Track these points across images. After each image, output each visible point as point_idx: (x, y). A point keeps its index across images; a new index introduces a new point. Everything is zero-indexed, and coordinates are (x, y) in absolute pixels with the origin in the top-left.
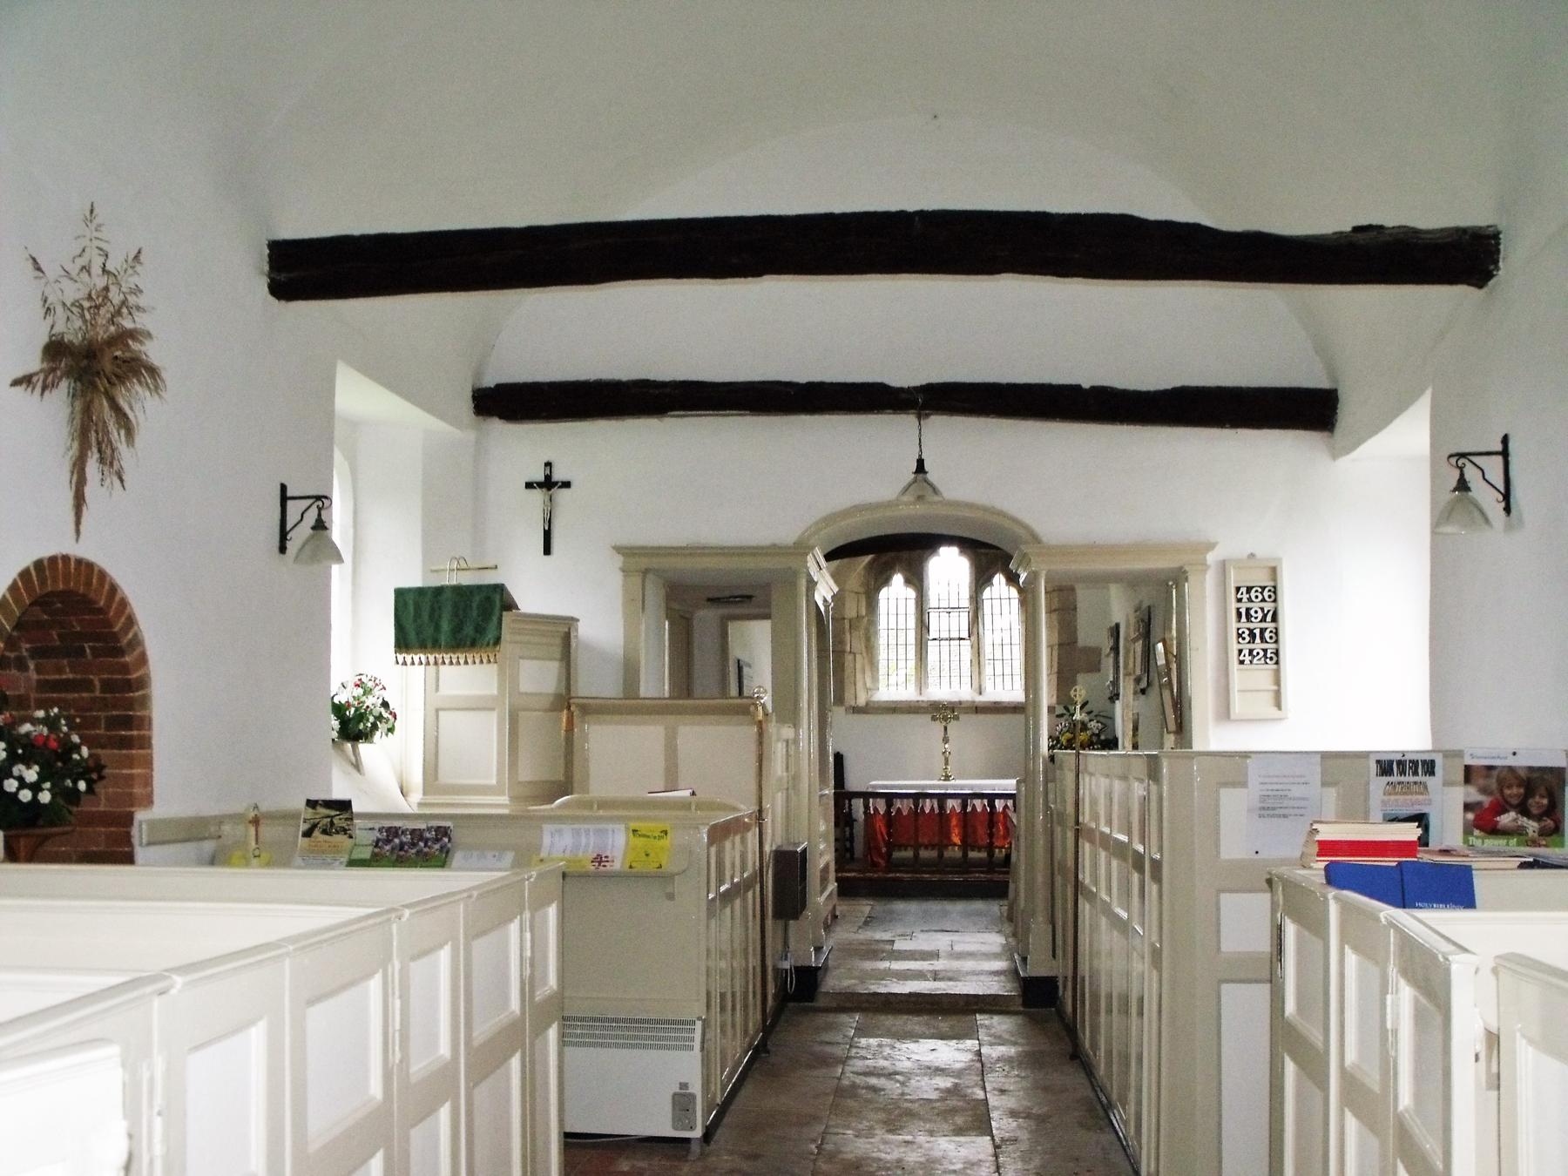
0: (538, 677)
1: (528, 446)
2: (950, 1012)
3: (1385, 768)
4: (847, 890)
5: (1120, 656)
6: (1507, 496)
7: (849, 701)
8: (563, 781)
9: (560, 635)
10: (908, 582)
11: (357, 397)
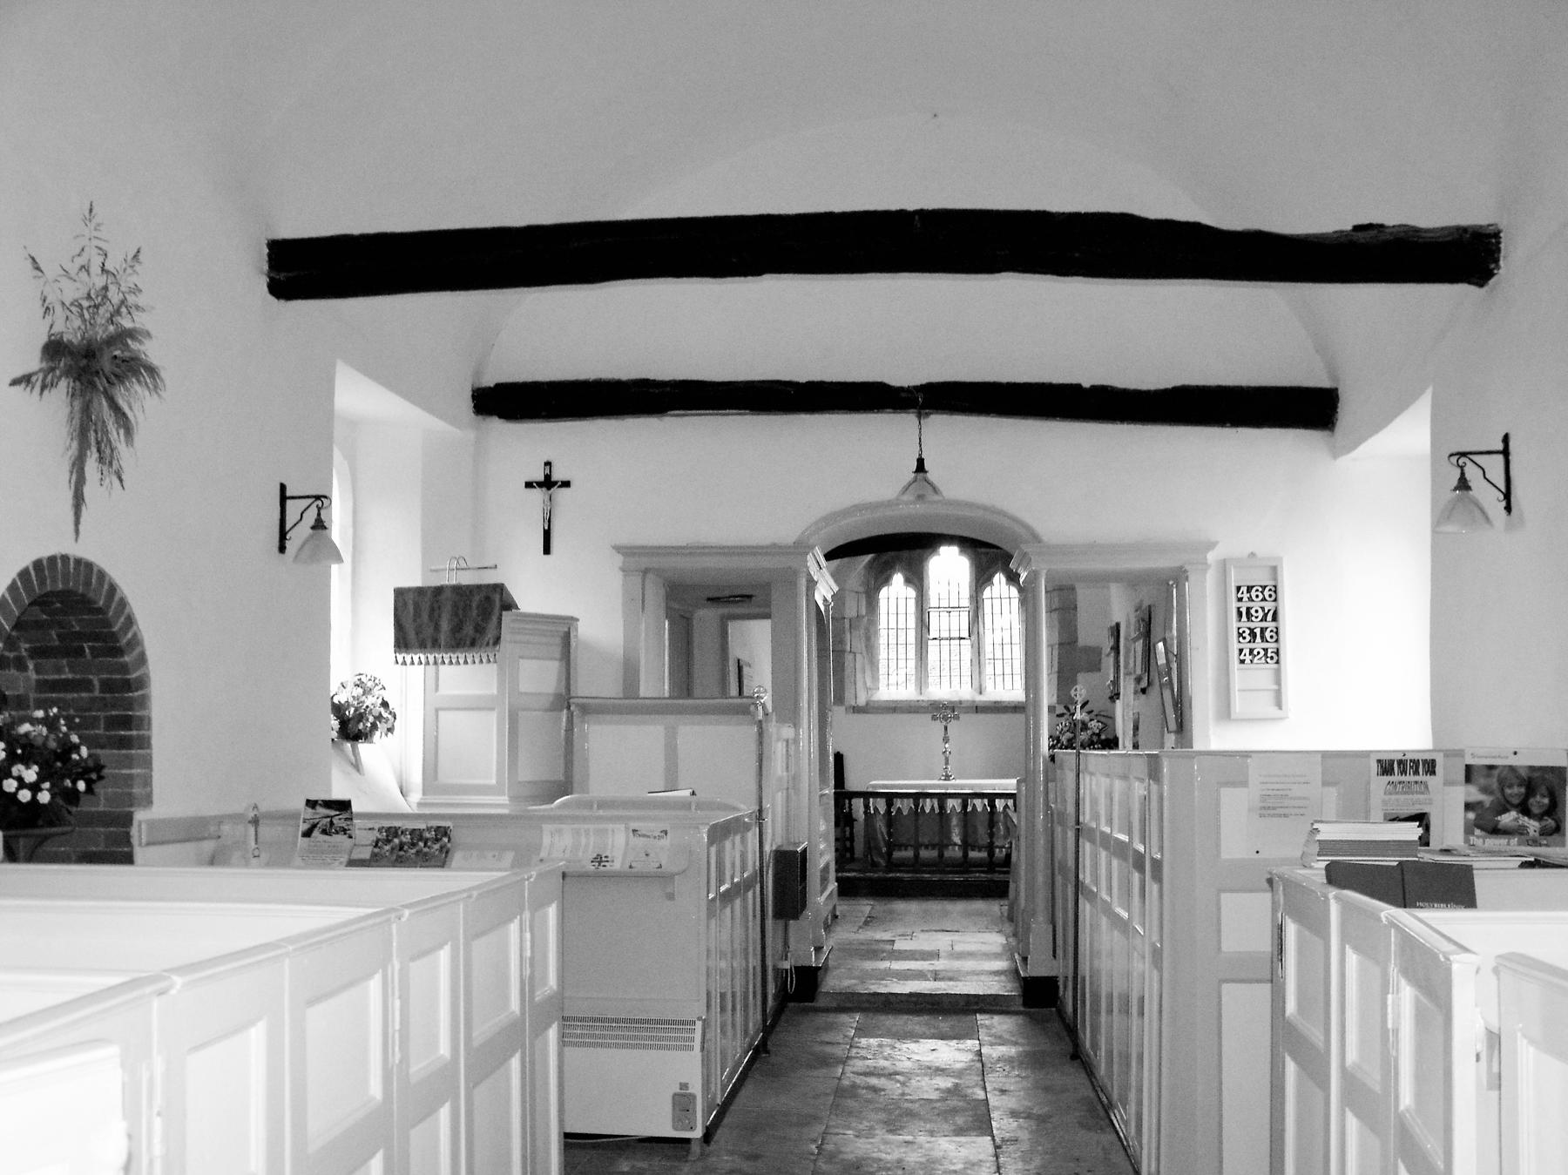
2: (950, 1011)
4: (848, 889)
6: (1507, 496)
7: (849, 699)
9: (561, 635)
10: (908, 581)
11: (357, 396)
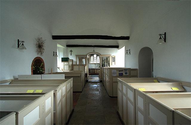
0: (71, 63)
1: (70, 49)
2: (95, 83)
3: (125, 70)
4: (89, 75)
5: (105, 61)
8: (72, 70)
9: (72, 61)
11: (58, 46)
